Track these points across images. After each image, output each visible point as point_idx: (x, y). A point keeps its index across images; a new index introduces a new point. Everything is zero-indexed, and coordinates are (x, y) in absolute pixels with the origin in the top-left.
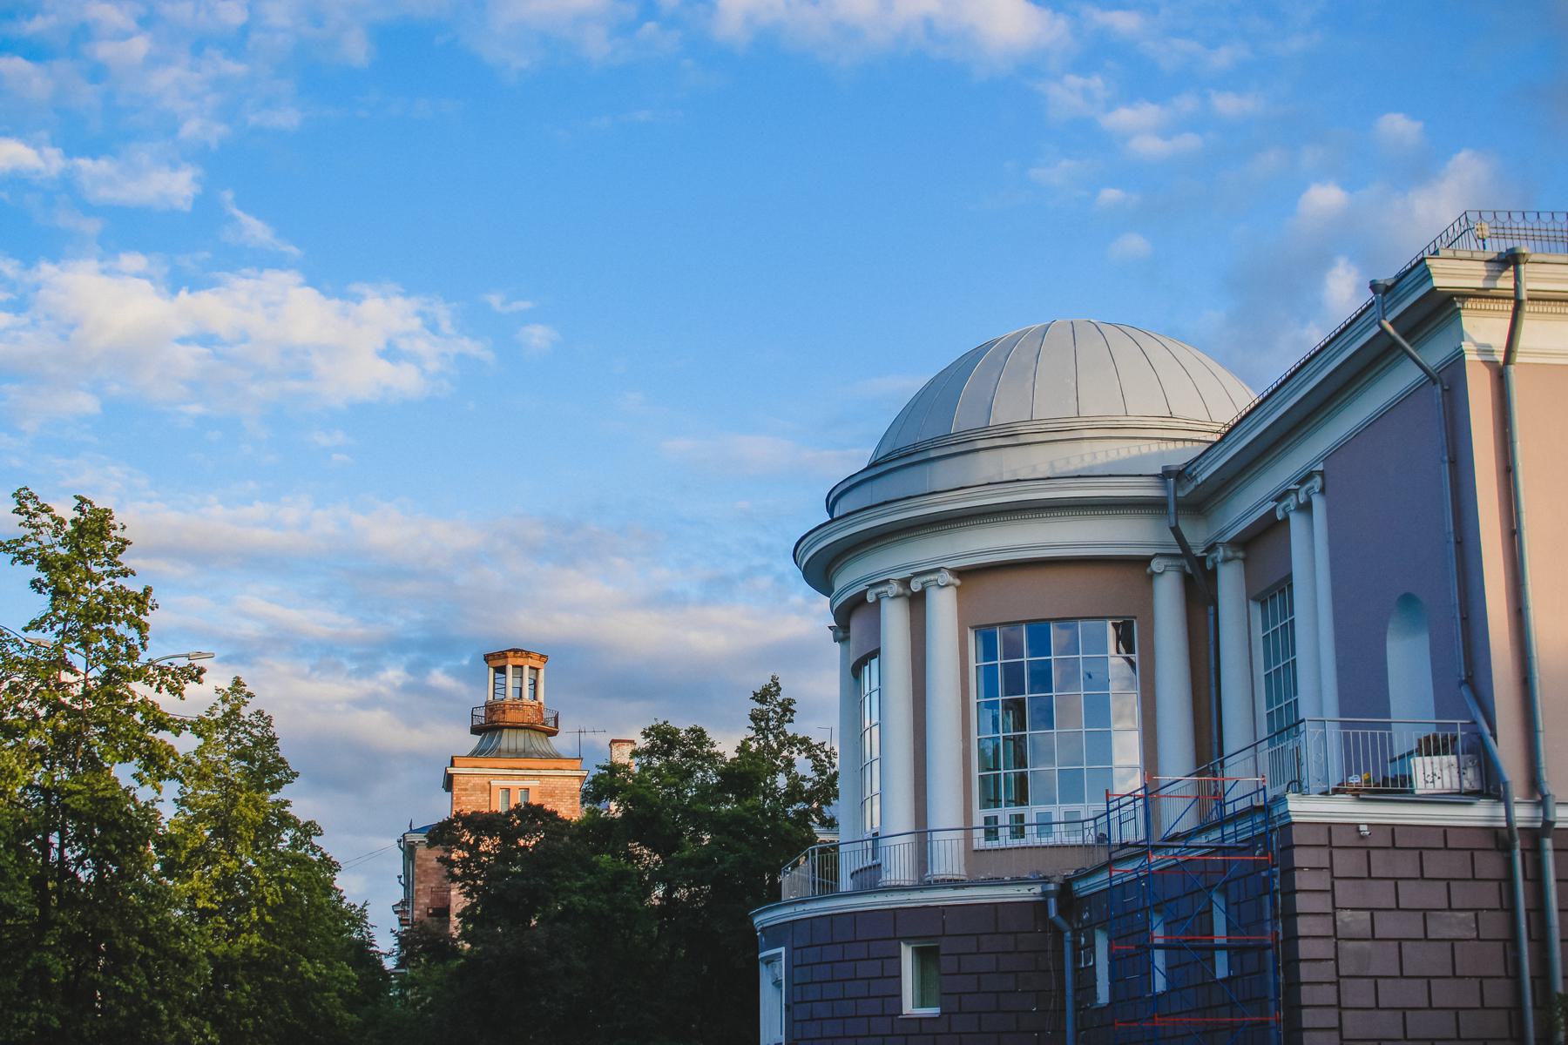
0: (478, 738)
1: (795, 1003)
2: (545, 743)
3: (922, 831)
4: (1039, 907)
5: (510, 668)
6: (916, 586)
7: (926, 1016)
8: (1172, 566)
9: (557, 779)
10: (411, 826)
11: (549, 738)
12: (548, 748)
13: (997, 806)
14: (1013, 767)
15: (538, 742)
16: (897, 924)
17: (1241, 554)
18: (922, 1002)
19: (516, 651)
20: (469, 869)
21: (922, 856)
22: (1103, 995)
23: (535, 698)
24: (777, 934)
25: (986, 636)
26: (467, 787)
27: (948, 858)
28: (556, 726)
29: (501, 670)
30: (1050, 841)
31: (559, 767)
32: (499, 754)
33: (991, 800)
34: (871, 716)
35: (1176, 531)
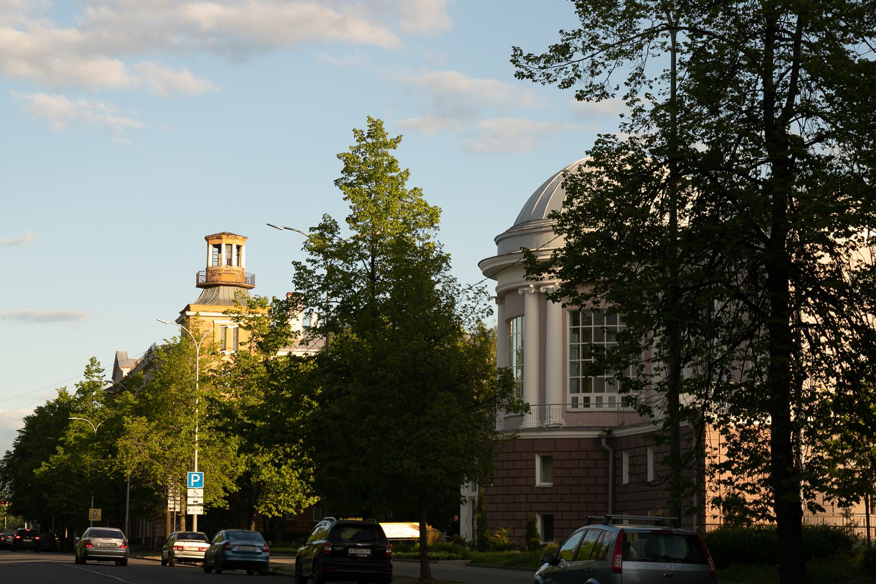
4: (597, 440)
5: (223, 247)
16: (534, 445)
18: (544, 479)
19: (229, 234)
22: (626, 480)
27: (556, 417)
29: (219, 247)
30: (600, 409)
34: (519, 344)
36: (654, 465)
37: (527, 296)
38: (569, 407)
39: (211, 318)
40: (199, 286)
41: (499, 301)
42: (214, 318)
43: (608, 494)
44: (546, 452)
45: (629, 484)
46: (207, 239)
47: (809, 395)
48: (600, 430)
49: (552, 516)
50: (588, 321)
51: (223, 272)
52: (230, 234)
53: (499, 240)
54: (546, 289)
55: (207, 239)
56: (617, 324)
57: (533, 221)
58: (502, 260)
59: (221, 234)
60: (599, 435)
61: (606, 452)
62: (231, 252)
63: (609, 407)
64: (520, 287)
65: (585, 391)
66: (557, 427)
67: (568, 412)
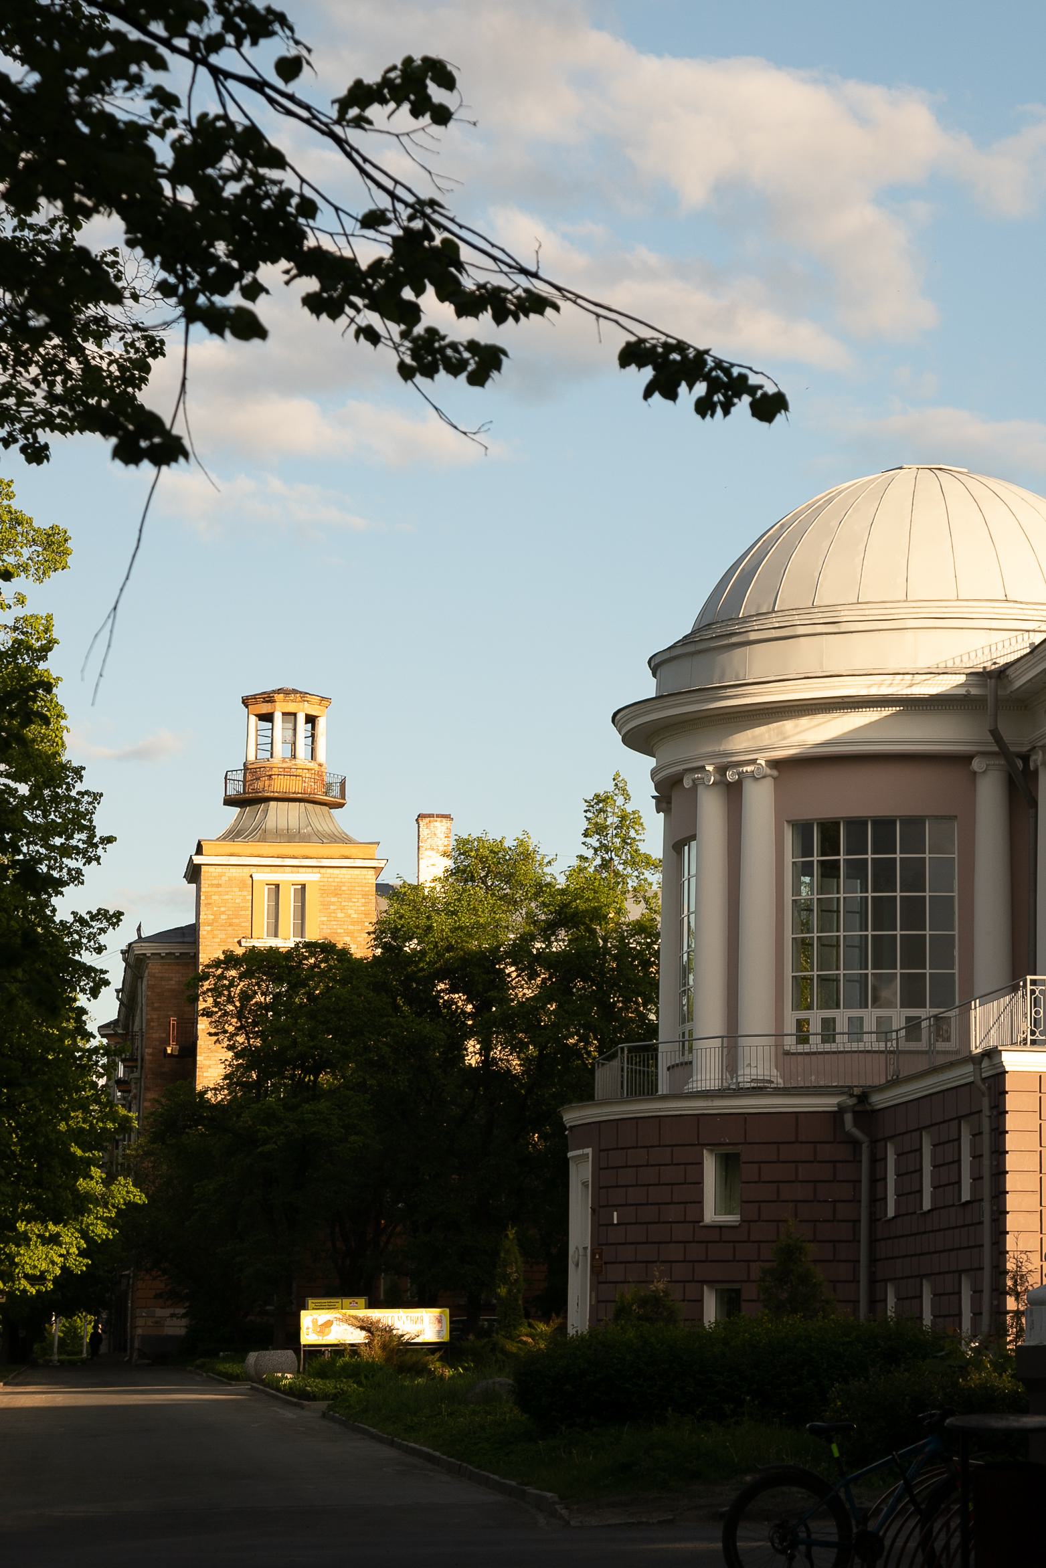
0: (235, 811)
1: (600, 1207)
3: (732, 1037)
4: (836, 1116)
5: (278, 717)
6: (731, 776)
10: (139, 929)
11: (332, 810)
12: (332, 827)
13: (838, 1007)
14: (858, 929)
15: (319, 818)
18: (725, 1206)
20: (19, 246)
21: (731, 1061)
25: (803, 830)
28: (343, 796)
29: (268, 718)
30: (861, 1046)
31: (347, 854)
32: (264, 836)
33: (802, 1003)
35: (995, 733)
36: (703, 1180)
37: (700, 789)
38: (790, 1043)
39: (246, 869)
41: (664, 805)
42: (253, 870)
46: (246, 702)
48: (843, 1093)
49: (738, 1291)
51: (275, 771)
52: (295, 692)
53: (657, 664)
54: (739, 774)
55: (246, 702)
56: (867, 854)
57: (713, 624)
58: (664, 708)
59: (274, 692)
60: (839, 1105)
61: (856, 1144)
62: (295, 730)
63: (824, 1041)
64: (686, 770)
65: (825, 1005)
66: (759, 1088)
67: (787, 1053)
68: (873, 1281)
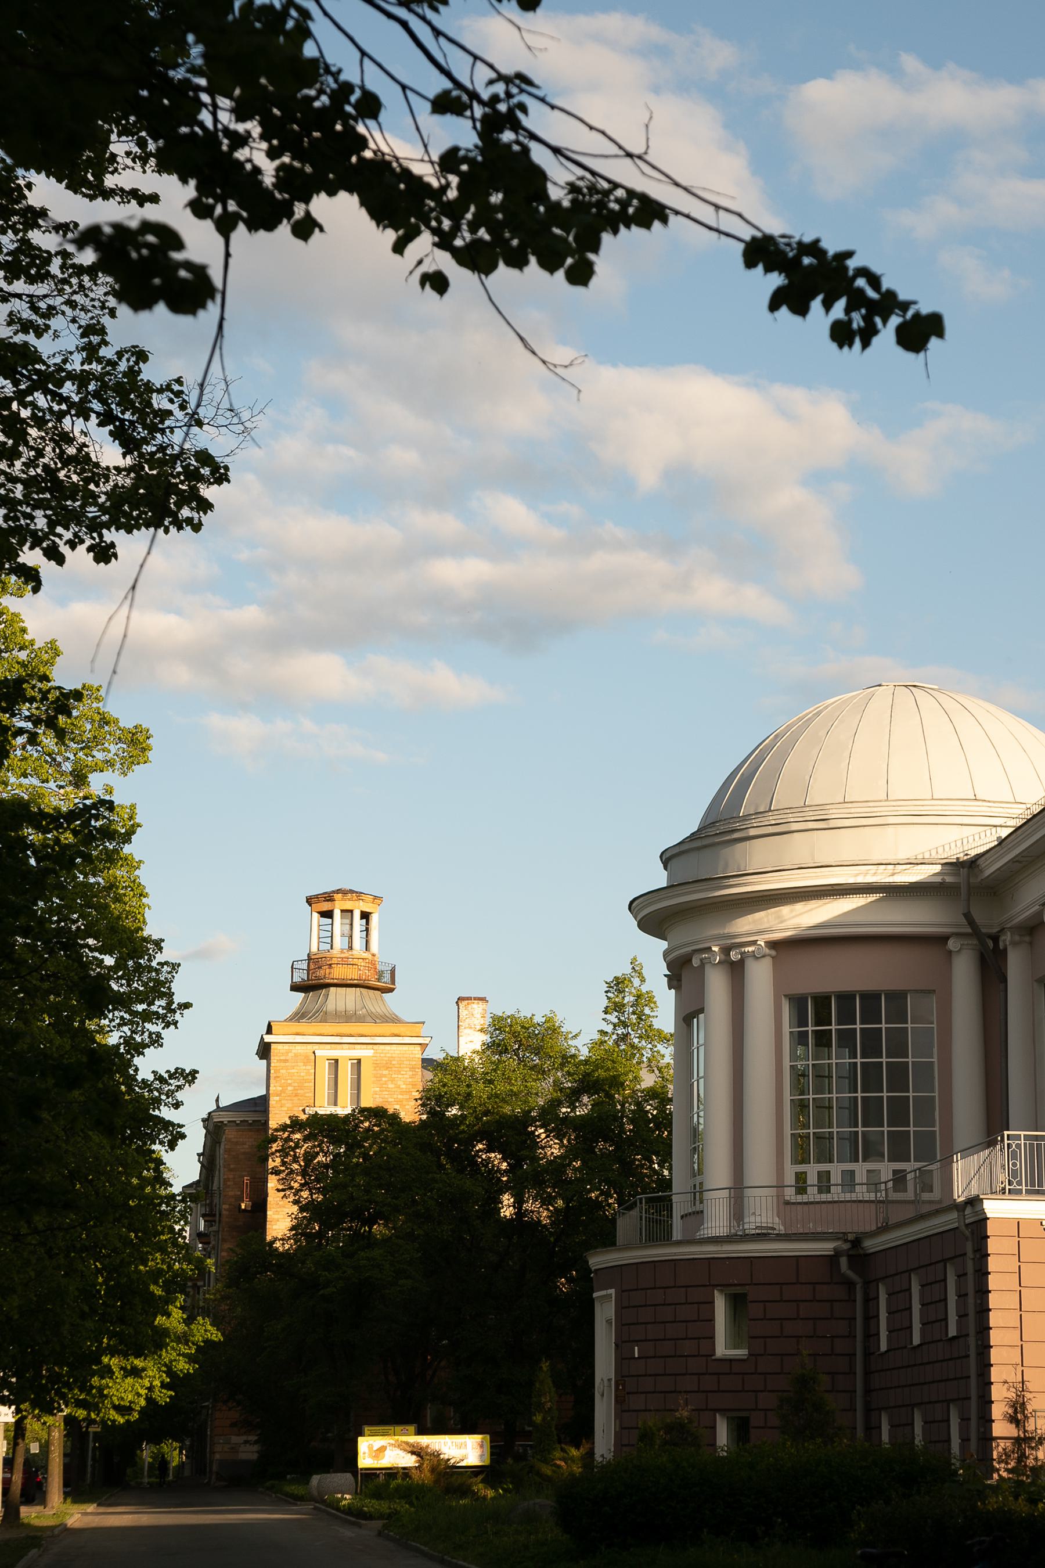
2: (380, 1002)
3: (738, 1189)
4: (832, 1260)
5: (337, 914)
6: (734, 956)
7: (737, 1357)
8: (967, 944)
9: (394, 1047)
10: (217, 1100)
15: (372, 1001)
17: (1027, 939)
18: (734, 1341)
19: (344, 892)
21: (738, 1209)
22: (883, 1347)
23: (367, 948)
24: (615, 1274)
25: (798, 1003)
26: (287, 1058)
28: (393, 982)
29: (328, 914)
30: (854, 1197)
31: (396, 1032)
32: (325, 1017)
33: (801, 1157)
35: (968, 916)
37: (708, 968)
38: (790, 1193)
39: (309, 1046)
40: (295, 988)
41: (675, 983)
42: (316, 1047)
43: (855, 1373)
44: (735, 1285)
45: (886, 1352)
46: (309, 901)
47: (556, 1141)
48: (838, 1239)
50: (847, 1017)
51: (335, 961)
52: (352, 892)
53: (668, 858)
54: (742, 954)
55: (309, 901)
59: (334, 892)
60: (835, 1249)
61: (850, 1285)
67: (787, 1203)
68: (868, 1410)
